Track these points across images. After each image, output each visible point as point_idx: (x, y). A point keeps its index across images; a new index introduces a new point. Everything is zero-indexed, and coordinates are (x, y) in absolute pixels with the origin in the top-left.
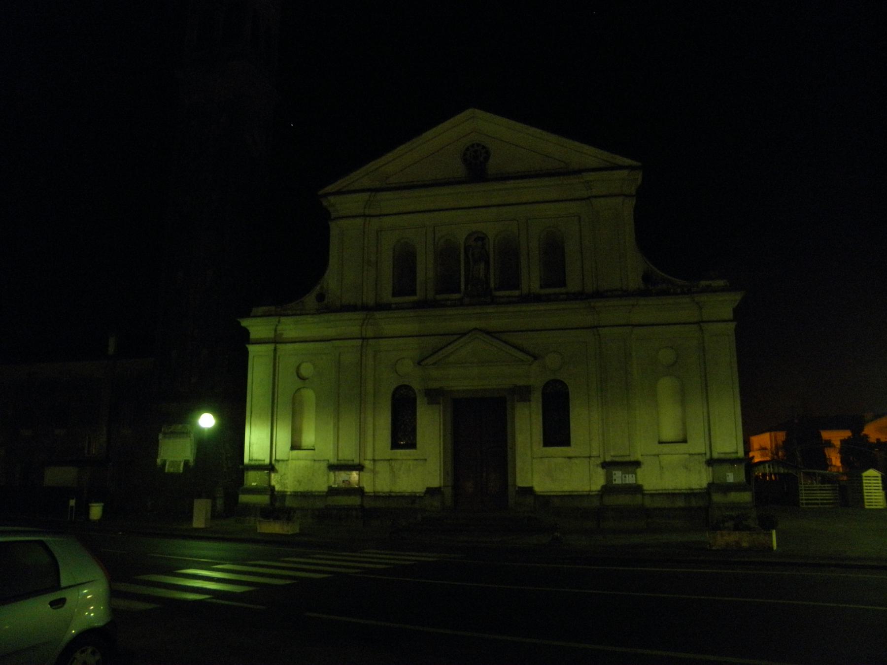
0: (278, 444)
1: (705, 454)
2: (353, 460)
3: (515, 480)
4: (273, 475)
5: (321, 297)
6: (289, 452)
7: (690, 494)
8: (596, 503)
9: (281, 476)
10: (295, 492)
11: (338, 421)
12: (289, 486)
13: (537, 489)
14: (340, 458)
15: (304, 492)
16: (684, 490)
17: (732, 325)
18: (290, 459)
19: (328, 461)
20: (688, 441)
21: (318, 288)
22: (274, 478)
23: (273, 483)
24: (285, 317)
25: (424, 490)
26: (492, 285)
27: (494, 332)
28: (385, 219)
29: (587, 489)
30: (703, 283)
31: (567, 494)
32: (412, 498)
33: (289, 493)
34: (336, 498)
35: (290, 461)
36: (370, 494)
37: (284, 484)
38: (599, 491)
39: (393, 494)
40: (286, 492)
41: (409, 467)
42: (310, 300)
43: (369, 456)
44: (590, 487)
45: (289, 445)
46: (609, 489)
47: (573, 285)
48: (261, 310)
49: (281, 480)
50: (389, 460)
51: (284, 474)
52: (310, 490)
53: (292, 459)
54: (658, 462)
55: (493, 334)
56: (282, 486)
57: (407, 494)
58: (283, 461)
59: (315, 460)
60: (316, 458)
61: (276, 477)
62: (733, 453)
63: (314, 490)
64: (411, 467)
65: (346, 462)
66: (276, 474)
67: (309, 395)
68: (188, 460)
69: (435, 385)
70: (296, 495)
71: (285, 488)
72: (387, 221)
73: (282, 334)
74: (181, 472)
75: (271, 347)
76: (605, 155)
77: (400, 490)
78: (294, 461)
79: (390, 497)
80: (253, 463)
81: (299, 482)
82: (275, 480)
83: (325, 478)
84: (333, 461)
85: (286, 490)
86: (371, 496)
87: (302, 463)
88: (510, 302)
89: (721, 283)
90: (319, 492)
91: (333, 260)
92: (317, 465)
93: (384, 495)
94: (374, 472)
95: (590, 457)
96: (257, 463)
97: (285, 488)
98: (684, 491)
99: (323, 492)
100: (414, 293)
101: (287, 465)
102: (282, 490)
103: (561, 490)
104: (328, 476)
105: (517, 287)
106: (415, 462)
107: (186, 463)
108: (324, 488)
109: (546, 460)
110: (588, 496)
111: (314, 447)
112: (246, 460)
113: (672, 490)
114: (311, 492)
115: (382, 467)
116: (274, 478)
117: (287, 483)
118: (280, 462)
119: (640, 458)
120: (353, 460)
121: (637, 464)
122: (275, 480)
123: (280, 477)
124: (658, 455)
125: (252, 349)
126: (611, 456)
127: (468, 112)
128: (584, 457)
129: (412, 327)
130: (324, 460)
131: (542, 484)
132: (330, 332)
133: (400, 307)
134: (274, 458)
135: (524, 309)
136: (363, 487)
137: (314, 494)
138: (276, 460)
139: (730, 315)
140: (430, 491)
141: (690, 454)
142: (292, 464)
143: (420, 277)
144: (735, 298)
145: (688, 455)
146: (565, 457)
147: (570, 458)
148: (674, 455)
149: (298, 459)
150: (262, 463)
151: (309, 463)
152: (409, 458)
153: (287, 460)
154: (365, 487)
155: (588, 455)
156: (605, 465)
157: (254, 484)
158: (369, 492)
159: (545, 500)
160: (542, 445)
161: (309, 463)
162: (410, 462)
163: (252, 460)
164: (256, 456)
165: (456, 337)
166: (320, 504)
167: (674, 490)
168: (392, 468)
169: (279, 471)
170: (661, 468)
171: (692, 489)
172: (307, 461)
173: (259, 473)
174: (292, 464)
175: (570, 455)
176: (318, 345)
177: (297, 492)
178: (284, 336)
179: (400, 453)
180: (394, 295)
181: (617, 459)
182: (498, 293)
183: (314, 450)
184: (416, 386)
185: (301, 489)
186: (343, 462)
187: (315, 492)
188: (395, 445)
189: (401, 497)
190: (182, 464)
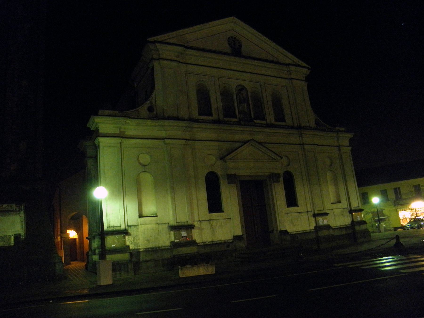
0: (128, 213)
1: (348, 208)
2: (187, 222)
3: (277, 227)
4: (127, 237)
5: (150, 109)
6: (138, 219)
7: (346, 228)
8: (314, 236)
9: (134, 238)
10: (146, 249)
11: (174, 195)
12: (141, 246)
13: (289, 231)
14: (178, 221)
15: (154, 248)
16: (344, 225)
17: (350, 148)
18: (139, 224)
19: (168, 223)
20: (342, 202)
21: (148, 102)
22: (128, 240)
23: (128, 243)
24: (130, 119)
25: (232, 238)
26: (253, 117)
27: (262, 143)
28: (190, 67)
29: (309, 229)
30: (337, 128)
31: (301, 232)
32: (226, 243)
33: (142, 250)
34: (180, 249)
35: (140, 226)
36: (201, 244)
37: (137, 244)
38: (314, 229)
39: (214, 243)
40: (140, 249)
41: (221, 223)
42: (143, 110)
43: (196, 219)
44: (310, 228)
45: (138, 214)
46: (318, 228)
47: (289, 122)
48: (107, 112)
49: (134, 240)
50: (209, 220)
51: (136, 236)
52: (157, 246)
53: (140, 224)
54: (333, 213)
55: (262, 144)
56: (135, 246)
57: (223, 242)
58: (134, 226)
59: (158, 224)
60: (159, 222)
61: (130, 238)
62: (358, 207)
63: (160, 245)
64: (223, 224)
65: (183, 224)
66: (130, 236)
67: (147, 178)
68: (20, 234)
69: (232, 172)
70: (148, 251)
71: (137, 246)
72: (190, 68)
73: (124, 132)
74: (12, 245)
75: (118, 140)
76: (296, 60)
77: (218, 239)
78: (143, 226)
79: (212, 244)
80: (111, 229)
81: (148, 240)
82: (129, 241)
83: (168, 236)
84: (173, 223)
85: (139, 248)
86: (201, 245)
87: (149, 226)
88: (261, 126)
89: (342, 129)
90: (164, 246)
91: (158, 86)
92: (160, 226)
93: (209, 244)
94: (201, 229)
95: (307, 212)
96: (115, 229)
97: (137, 246)
98: (344, 226)
99: (167, 246)
100: (211, 115)
101: (138, 229)
102: (136, 248)
103: (298, 231)
104: (169, 234)
105: (264, 119)
106: (225, 221)
107: (17, 237)
108: (167, 243)
109: (290, 214)
110: (309, 232)
111: (156, 214)
112: (105, 228)
113: (340, 226)
114: (159, 247)
115: (205, 225)
116: (128, 240)
117: (139, 243)
118: (132, 227)
119: (327, 212)
120: (187, 222)
121: (326, 214)
122: (129, 241)
123: (132, 238)
124: (332, 209)
125: (102, 141)
126: (317, 211)
127: (232, 18)
128: (305, 212)
129: (212, 135)
130: (165, 224)
131: (291, 229)
132: (163, 134)
133: (204, 122)
134: (126, 225)
135: (272, 131)
136: (195, 240)
137: (161, 248)
138: (128, 226)
139: (348, 144)
140: (236, 238)
141: (343, 208)
142: (141, 228)
143: (214, 106)
144: (350, 135)
145: (342, 209)
146: (297, 213)
147: (300, 213)
148: (338, 209)
149: (146, 224)
150: (119, 228)
151: (154, 226)
152: (220, 218)
153: (138, 225)
154: (196, 240)
155: (306, 211)
156: (315, 216)
157: (113, 246)
158: (200, 243)
159: (294, 236)
160: (286, 206)
161: (154, 226)
162: (222, 221)
163: (109, 227)
164: (112, 224)
165: (239, 144)
166: (167, 255)
167: (341, 226)
168: (211, 226)
169: (132, 233)
170: (335, 215)
171: (346, 225)
172: (153, 225)
173: (117, 236)
174: (141, 228)
175: (299, 211)
176: (157, 142)
177: (149, 248)
178: (126, 133)
179: (215, 215)
180: (200, 114)
181: (319, 212)
182: (256, 121)
183: (157, 216)
184: (219, 173)
185: (150, 246)
186: (180, 224)
187: (161, 247)
188: (362, 193)
189: (219, 244)
190: (13, 238)
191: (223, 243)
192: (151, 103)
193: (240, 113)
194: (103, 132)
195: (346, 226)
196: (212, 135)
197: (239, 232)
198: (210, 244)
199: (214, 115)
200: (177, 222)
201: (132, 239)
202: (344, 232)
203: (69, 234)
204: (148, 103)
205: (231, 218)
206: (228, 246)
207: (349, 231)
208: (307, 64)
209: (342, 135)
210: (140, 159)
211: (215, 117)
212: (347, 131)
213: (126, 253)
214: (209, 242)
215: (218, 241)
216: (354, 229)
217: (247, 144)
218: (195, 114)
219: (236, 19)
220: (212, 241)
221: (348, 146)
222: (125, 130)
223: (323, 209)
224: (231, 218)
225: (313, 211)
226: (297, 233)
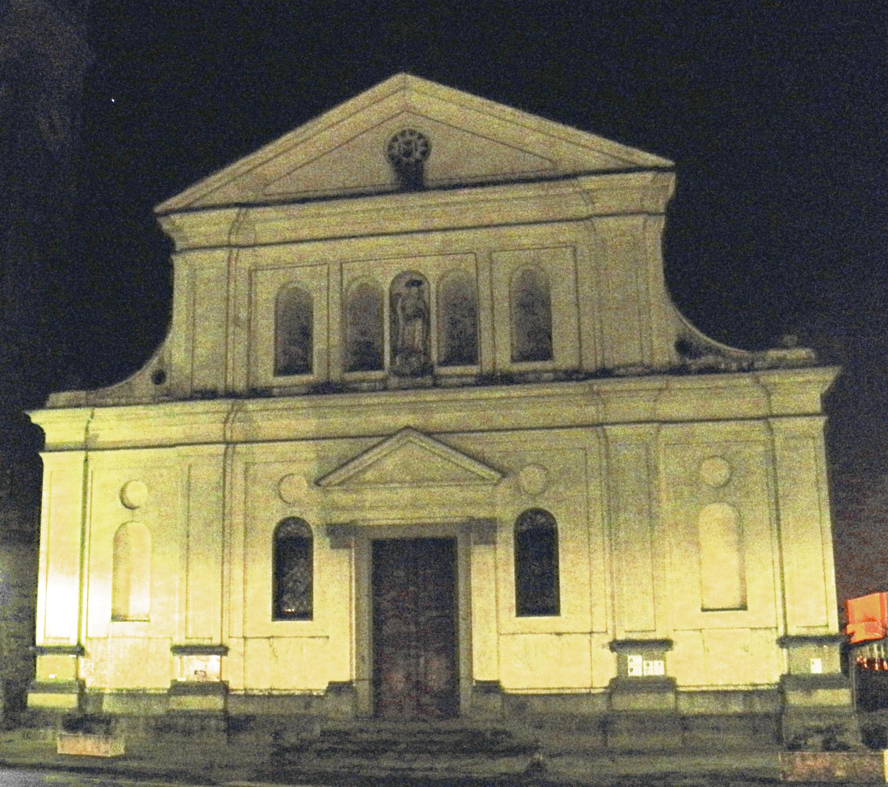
5: (159, 377)
8: (601, 706)
33: (108, 691)
39: (275, 693)
42: (142, 380)
53: (113, 637)
57: (297, 693)
61: (88, 665)
69: (343, 518)
72: (269, 254)
73: (97, 436)
85: (103, 686)
93: (261, 694)
116: (85, 667)
129: (309, 425)
139: (818, 407)
140: (336, 688)
143: (318, 346)
144: (827, 376)
156: (616, 646)
160: (514, 613)
166: (158, 709)
180: (278, 372)
183: (149, 621)
184: (312, 518)
191: (297, 696)
192: (161, 361)
193: (395, 351)
194: (52, 441)
195: (751, 688)
196: (309, 425)
197: (345, 672)
198: (264, 696)
199: (315, 368)
200: (187, 638)
201: (93, 667)
202: (736, 707)
203: (675, 679)
204: (154, 363)
205: (328, 637)
206: (308, 705)
207: (771, 707)
208: (651, 150)
209: (607, 388)
210: (721, 480)
211: (316, 375)
212: (821, 362)
213: (71, 693)
214: (261, 691)
215: (285, 690)
216: (784, 700)
217: (394, 439)
218: (266, 375)
219: (410, 77)
220: (271, 689)
221: (818, 415)
222: (98, 432)
223: (654, 629)
224: (328, 637)
225: (610, 632)
226: (539, 693)
